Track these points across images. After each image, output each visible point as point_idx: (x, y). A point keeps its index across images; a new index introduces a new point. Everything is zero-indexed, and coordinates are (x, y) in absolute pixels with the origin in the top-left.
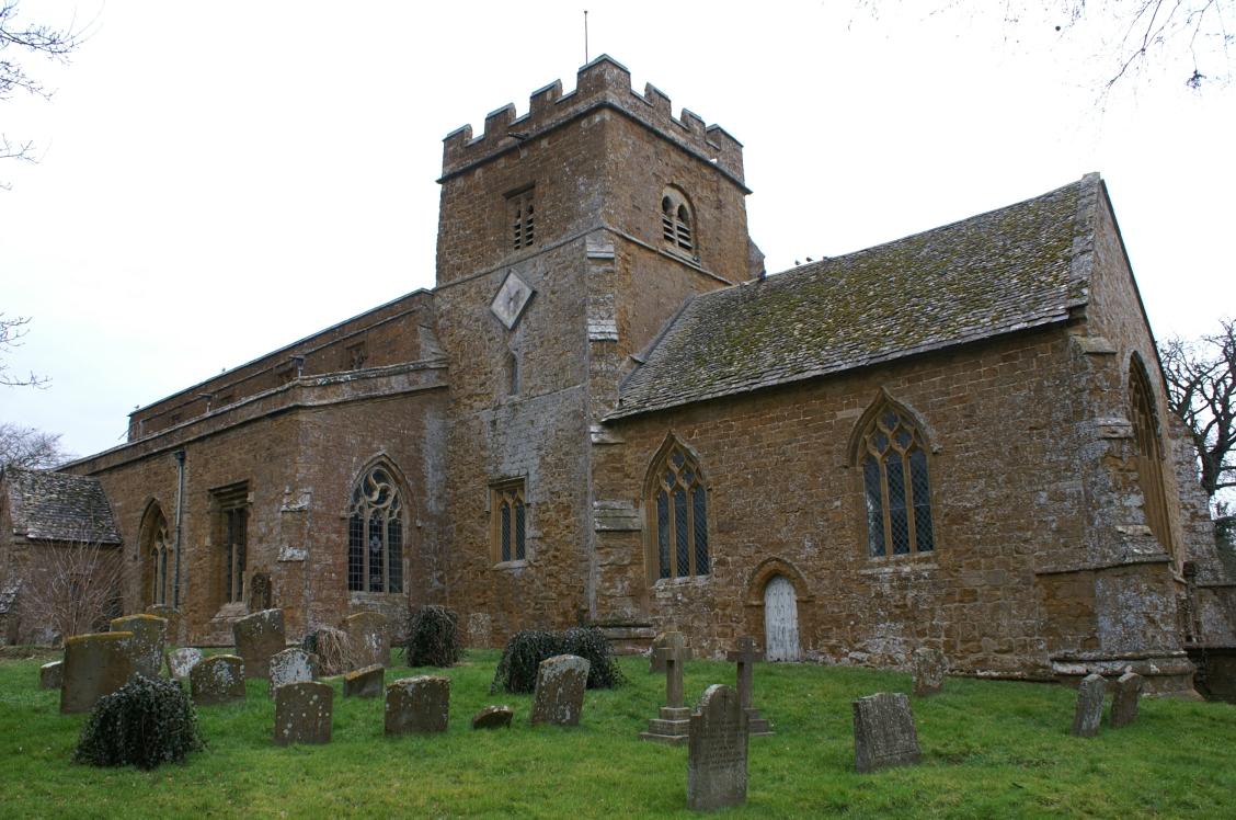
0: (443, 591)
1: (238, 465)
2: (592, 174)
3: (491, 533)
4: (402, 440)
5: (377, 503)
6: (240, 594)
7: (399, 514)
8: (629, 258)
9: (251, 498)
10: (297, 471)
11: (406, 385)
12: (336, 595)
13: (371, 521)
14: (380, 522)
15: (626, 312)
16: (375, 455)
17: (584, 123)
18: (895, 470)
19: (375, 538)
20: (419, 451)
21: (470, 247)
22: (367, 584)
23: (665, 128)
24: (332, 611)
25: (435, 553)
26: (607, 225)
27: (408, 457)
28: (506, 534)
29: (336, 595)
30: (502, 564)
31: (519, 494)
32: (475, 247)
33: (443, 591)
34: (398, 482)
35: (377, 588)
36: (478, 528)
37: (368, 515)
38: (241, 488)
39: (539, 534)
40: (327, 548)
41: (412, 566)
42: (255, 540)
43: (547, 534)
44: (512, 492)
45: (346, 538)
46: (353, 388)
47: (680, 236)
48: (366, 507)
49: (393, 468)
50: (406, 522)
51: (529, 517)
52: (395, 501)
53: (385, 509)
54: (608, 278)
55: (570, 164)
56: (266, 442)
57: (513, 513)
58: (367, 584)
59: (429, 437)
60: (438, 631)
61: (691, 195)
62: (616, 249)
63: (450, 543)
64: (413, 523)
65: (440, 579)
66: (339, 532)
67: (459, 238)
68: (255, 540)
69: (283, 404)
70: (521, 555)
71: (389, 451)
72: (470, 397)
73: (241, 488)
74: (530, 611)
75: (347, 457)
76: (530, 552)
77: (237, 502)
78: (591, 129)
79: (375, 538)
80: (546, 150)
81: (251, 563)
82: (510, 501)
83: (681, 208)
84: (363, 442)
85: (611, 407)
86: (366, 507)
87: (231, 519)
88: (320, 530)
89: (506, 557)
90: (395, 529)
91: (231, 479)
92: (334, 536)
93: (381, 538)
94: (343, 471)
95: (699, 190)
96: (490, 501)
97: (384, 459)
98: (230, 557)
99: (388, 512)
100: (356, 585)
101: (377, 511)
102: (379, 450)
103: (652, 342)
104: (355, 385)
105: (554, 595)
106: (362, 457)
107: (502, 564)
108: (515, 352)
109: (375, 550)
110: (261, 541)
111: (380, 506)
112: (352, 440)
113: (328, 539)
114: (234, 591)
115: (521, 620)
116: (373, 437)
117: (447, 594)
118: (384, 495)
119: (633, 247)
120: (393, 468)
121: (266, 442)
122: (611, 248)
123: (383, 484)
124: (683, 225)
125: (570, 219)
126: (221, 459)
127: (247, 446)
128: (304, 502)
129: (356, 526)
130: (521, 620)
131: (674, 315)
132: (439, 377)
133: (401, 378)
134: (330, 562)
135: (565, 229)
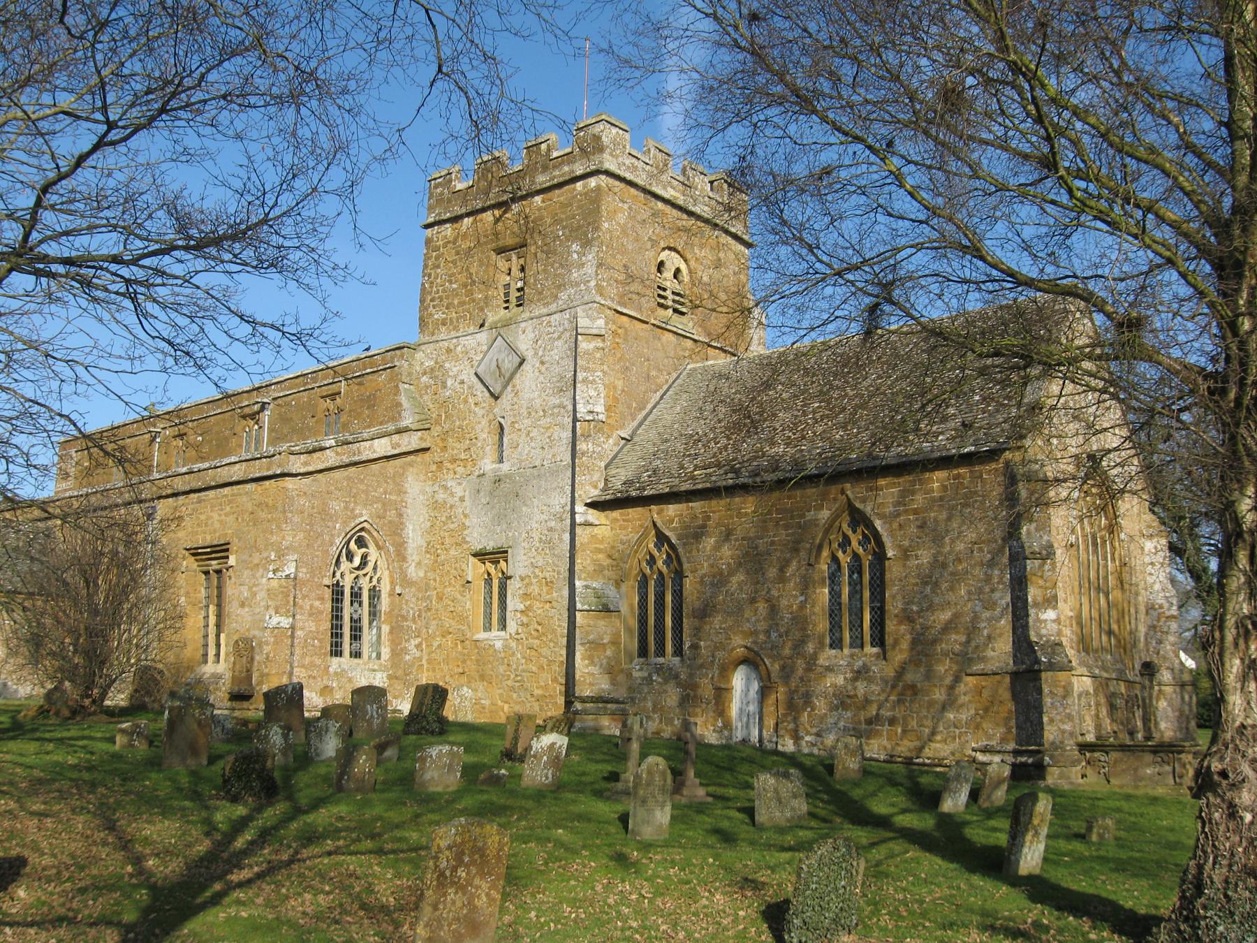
0: (420, 659)
1: (217, 525)
2: (587, 244)
3: (473, 603)
4: (384, 504)
5: (357, 569)
6: (218, 655)
7: (379, 581)
8: (620, 331)
9: (232, 561)
10: (283, 538)
11: (389, 448)
12: (318, 662)
13: (352, 588)
14: (360, 589)
15: (615, 388)
16: (357, 521)
17: (579, 185)
18: (856, 567)
19: (356, 605)
20: (400, 515)
21: (456, 302)
22: (347, 652)
23: (665, 188)
24: (314, 678)
25: (414, 620)
26: (598, 299)
27: (390, 522)
28: (488, 605)
29: (318, 662)
30: (482, 635)
31: (503, 564)
32: (462, 304)
33: (420, 659)
34: (379, 548)
35: (357, 654)
36: (459, 597)
37: (347, 583)
38: (221, 550)
39: (522, 607)
40: (310, 615)
41: (391, 632)
42: (235, 604)
43: (528, 608)
44: (496, 562)
45: (329, 605)
46: (337, 454)
47: (674, 301)
48: (347, 573)
49: (375, 534)
50: (385, 588)
51: (512, 586)
52: (375, 568)
53: (365, 575)
54: (598, 355)
55: (564, 228)
56: (249, 506)
57: (496, 583)
58: (347, 652)
59: (410, 501)
60: (1064, 697)
61: (689, 256)
62: (607, 323)
63: (429, 610)
64: (393, 589)
65: (418, 646)
66: (322, 599)
67: (444, 291)
68: (235, 604)
69: (268, 469)
70: (503, 625)
71: (371, 517)
72: (454, 461)
73: (221, 550)
74: (509, 683)
75: (330, 524)
76: (512, 626)
77: (214, 562)
78: (586, 194)
79: (356, 605)
80: (539, 209)
81: (231, 625)
82: (492, 571)
83: (678, 271)
84: (346, 508)
85: (596, 487)
86: (347, 573)
87: (208, 579)
88: (304, 597)
89: (488, 628)
90: (374, 594)
91: (209, 539)
92: (317, 603)
93: (360, 604)
94: (327, 538)
95: (697, 251)
96: (475, 570)
97: (365, 525)
98: (207, 617)
99: (368, 577)
100: (336, 652)
101: (357, 577)
102: (361, 515)
103: (640, 417)
104: (339, 449)
105: (534, 669)
106: (345, 523)
107: (482, 635)
108: (502, 420)
109: (355, 617)
110: (242, 605)
111: (361, 573)
112: (336, 506)
113: (311, 606)
114: (212, 652)
115: (500, 691)
116: (355, 502)
117: (424, 662)
118: (364, 563)
119: (625, 319)
120: (375, 534)
121: (249, 506)
122: (601, 322)
123: (364, 550)
124: (678, 288)
125: (562, 287)
126: (198, 518)
127: (228, 509)
128: (290, 569)
129: (337, 592)
130: (500, 691)
131: (665, 387)
132: (421, 439)
133: (383, 440)
134: (313, 629)
135: (556, 296)
